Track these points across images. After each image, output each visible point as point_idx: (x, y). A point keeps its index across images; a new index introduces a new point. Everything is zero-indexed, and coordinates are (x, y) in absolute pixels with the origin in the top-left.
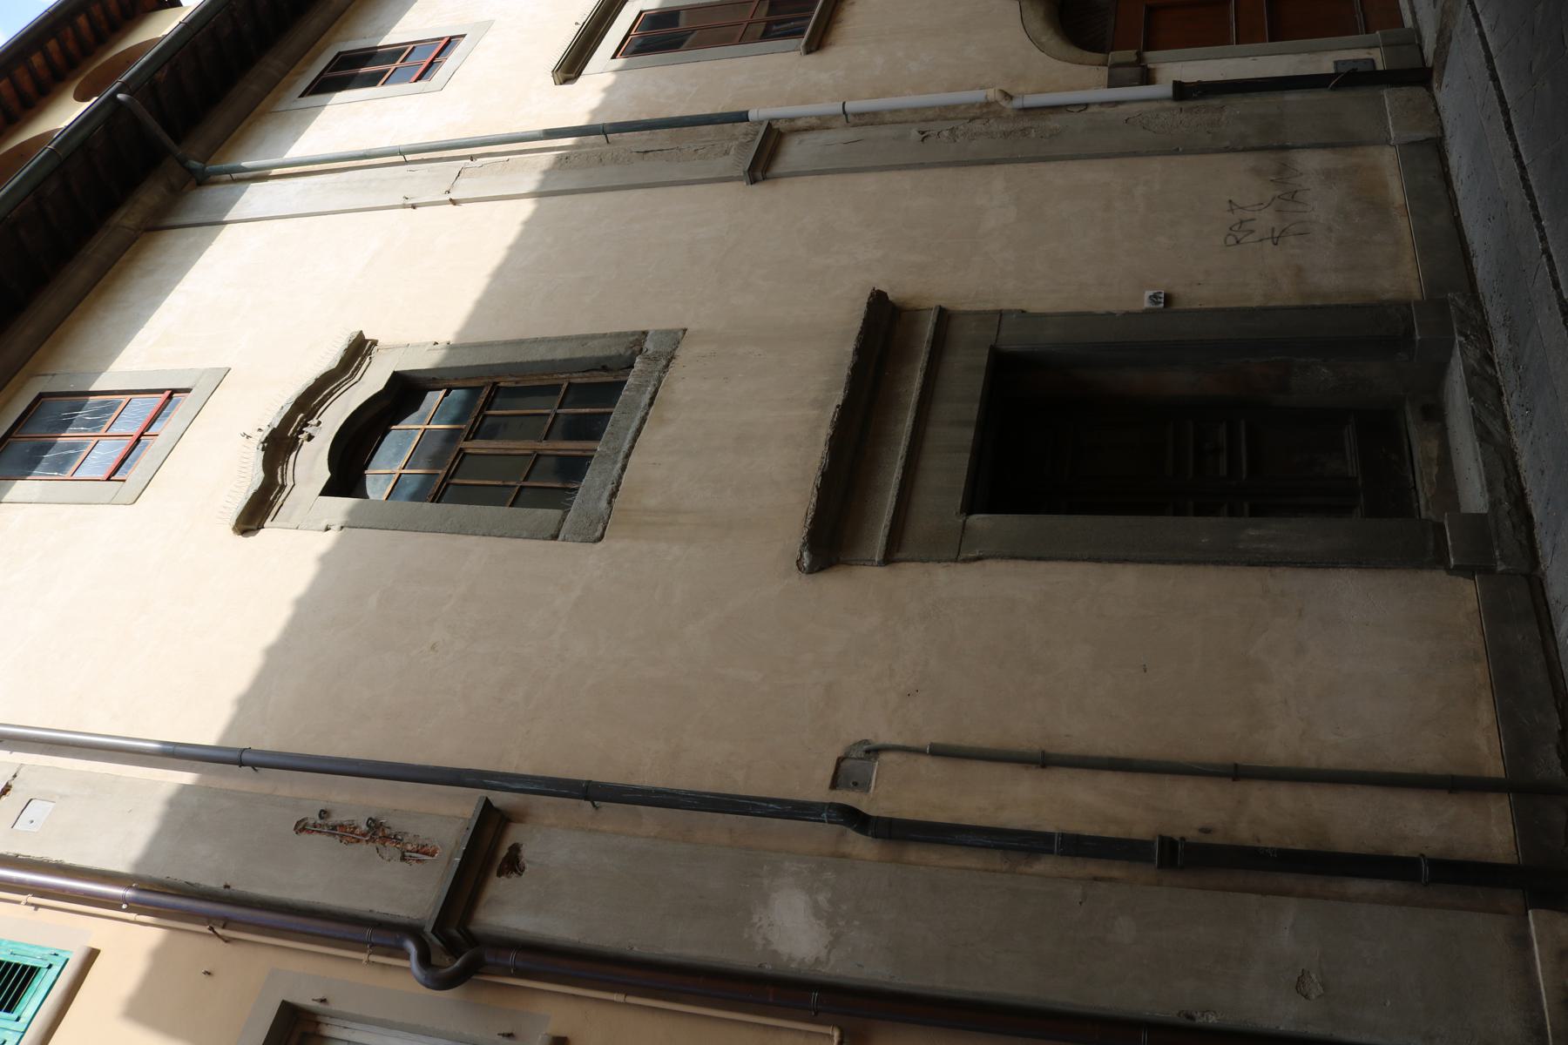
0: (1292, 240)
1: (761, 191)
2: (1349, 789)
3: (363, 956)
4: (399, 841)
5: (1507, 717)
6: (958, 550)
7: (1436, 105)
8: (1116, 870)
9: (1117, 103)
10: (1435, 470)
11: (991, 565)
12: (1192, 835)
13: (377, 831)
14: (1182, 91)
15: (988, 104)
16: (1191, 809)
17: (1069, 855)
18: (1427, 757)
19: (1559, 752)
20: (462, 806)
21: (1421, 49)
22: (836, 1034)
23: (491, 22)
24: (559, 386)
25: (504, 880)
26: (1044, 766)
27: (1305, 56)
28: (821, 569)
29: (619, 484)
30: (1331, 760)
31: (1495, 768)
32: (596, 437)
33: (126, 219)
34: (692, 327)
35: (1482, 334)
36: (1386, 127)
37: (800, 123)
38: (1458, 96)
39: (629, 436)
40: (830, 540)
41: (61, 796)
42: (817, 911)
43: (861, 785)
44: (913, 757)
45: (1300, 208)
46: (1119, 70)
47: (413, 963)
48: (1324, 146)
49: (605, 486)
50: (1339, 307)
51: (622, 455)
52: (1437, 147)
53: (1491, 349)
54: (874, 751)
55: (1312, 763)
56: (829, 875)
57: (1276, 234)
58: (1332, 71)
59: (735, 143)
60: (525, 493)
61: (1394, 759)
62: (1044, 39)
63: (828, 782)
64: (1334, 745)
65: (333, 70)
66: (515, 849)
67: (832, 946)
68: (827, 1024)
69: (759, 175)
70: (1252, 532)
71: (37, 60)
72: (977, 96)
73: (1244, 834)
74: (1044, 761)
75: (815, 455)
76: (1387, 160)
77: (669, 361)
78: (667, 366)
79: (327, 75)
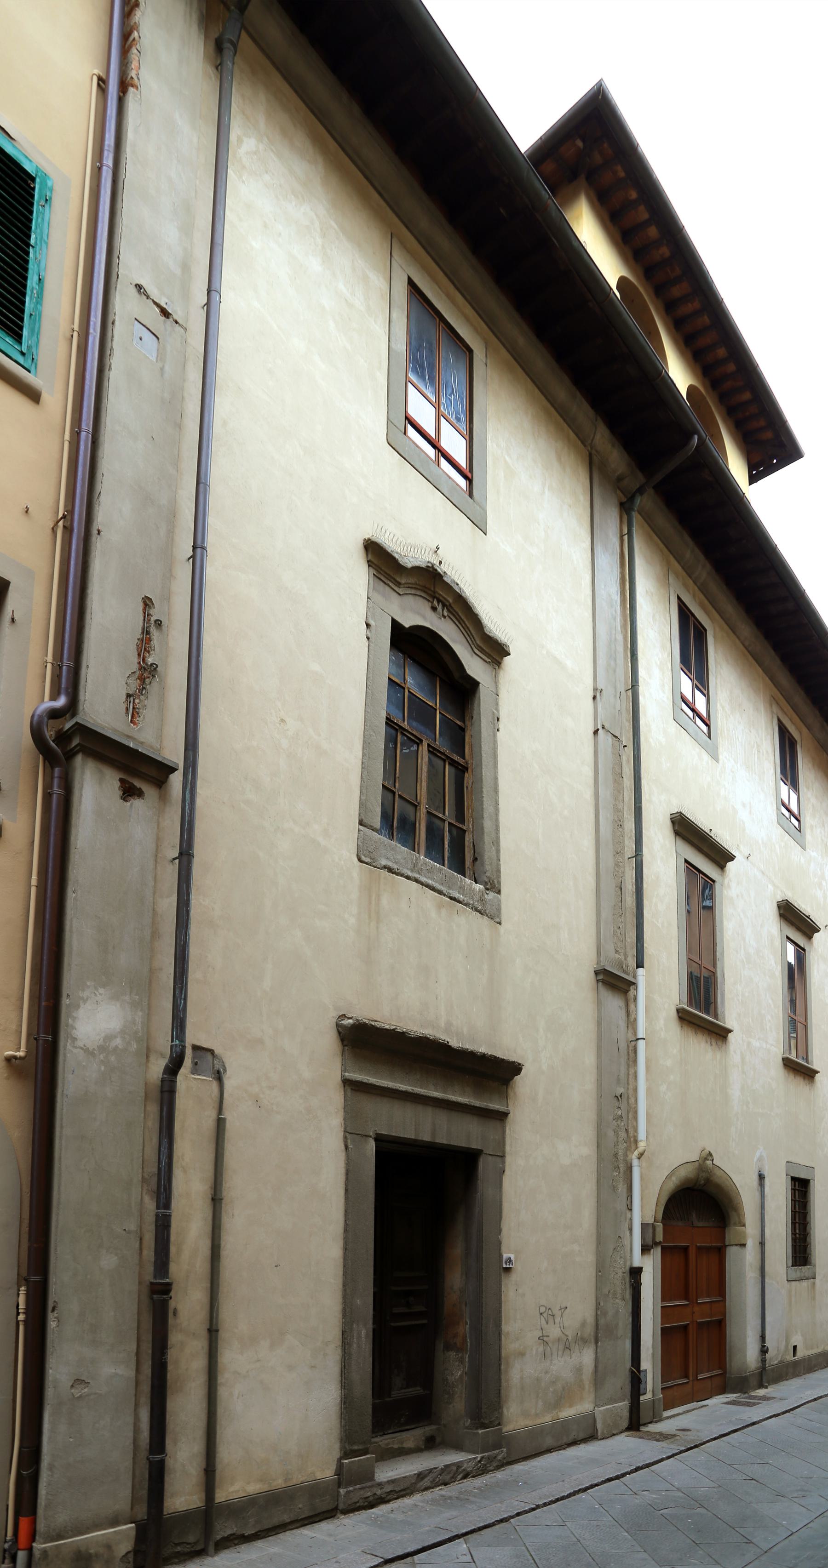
0: (541, 1349)
1: (587, 976)
2: (204, 1405)
3: (50, 658)
4: (141, 691)
5: (251, 1502)
6: (352, 1134)
7: (617, 1434)
8: (149, 1254)
9: (631, 1230)
10: (396, 1446)
11: (342, 1156)
12: (172, 1304)
13: (147, 672)
14: (636, 1273)
15: (636, 1141)
16: (189, 1303)
17: (157, 1221)
18: (226, 1454)
19: (231, 1535)
20: (172, 752)
21: (651, 1423)
22: (21, 1054)
23: (717, 761)
24: (463, 822)
25: (117, 784)
26: (213, 1199)
27: (651, 1351)
28: (339, 1033)
29: (397, 874)
30: (223, 1392)
31: (221, 1496)
32: (428, 855)
33: (602, 437)
34: (502, 929)
35: (482, 1470)
36: (606, 1404)
37: (632, 1006)
38: (627, 1448)
39: (430, 882)
40: (363, 1041)
41: (162, 369)
42: (108, 1038)
43: (196, 1068)
44: (217, 1105)
45: (560, 1353)
46: (651, 1230)
47: (48, 704)
48: (596, 1367)
49: (396, 863)
50: (500, 1380)
51: (417, 876)
52: (592, 1437)
53: (473, 1477)
54: (219, 1077)
55: (221, 1379)
56: (134, 1046)
57: (545, 1339)
58: (642, 1368)
59: (623, 958)
60: (390, 796)
61: (226, 1434)
62: (674, 1178)
63: (198, 1043)
64: (234, 1395)
65: (694, 624)
66: (139, 794)
67: (86, 1050)
68: (27, 1048)
69: (601, 977)
70: (363, 1333)
71: (722, 352)
72: (642, 1135)
73: (175, 1338)
74: (216, 1200)
75: (415, 1027)
76: (583, 1406)
77: (480, 912)
78: (476, 910)
79: (692, 619)
